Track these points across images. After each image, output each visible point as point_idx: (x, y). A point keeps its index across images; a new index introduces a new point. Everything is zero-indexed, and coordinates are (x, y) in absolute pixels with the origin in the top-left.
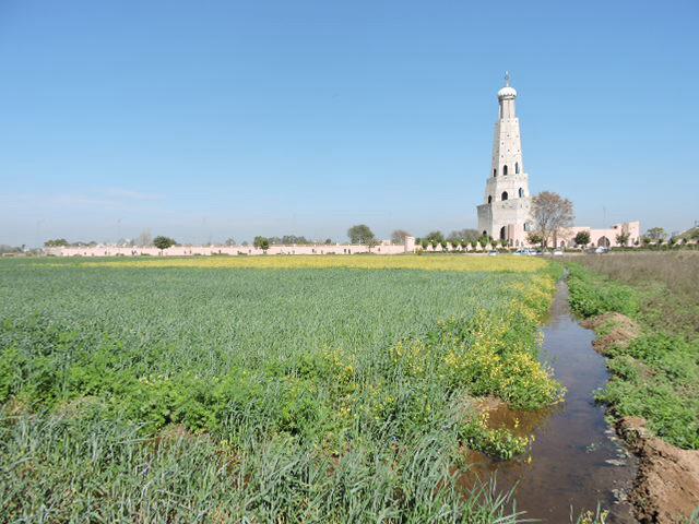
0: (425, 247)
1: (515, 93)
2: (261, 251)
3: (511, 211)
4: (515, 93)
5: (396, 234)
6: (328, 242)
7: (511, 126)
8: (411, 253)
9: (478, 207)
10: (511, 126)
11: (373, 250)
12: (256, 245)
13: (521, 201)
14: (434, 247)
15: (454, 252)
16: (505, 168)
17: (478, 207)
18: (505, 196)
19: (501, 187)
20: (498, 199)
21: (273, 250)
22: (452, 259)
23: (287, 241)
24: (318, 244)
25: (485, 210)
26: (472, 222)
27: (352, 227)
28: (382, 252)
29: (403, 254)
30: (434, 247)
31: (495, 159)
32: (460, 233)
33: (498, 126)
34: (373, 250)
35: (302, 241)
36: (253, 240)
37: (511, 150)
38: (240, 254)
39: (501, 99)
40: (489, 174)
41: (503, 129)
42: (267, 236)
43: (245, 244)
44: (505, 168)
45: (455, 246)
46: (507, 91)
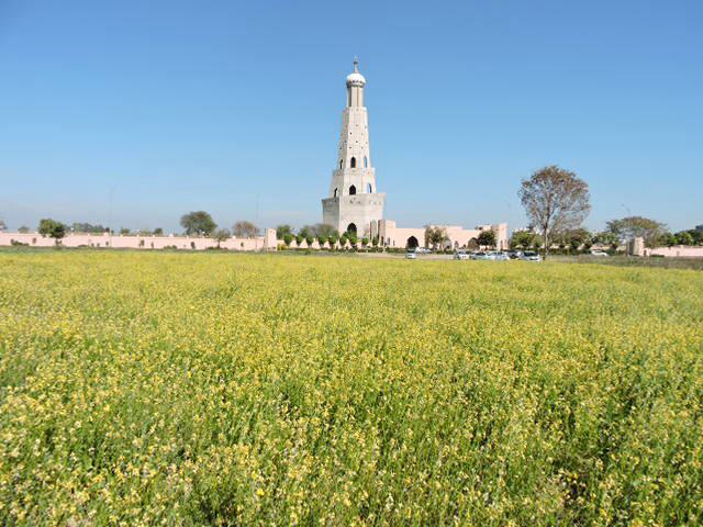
0: (288, 242)
1: (364, 81)
2: (50, 241)
3: (360, 207)
4: (364, 81)
5: (239, 226)
6: (158, 232)
7: (359, 116)
8: (271, 252)
9: (324, 202)
10: (359, 116)
11: (223, 245)
12: (43, 232)
13: (369, 197)
14: (298, 243)
15: (342, 251)
16: (353, 160)
17: (324, 202)
18: (353, 190)
19: (348, 180)
20: (346, 192)
21: (70, 240)
22: (304, 262)
23: (87, 229)
24: (147, 234)
25: (331, 205)
26: (314, 217)
27: (189, 214)
28: (246, 248)
29: (262, 251)
30: (298, 243)
31: (343, 148)
32: (313, 229)
33: (346, 114)
34: (223, 245)
35: (99, 230)
36: (38, 225)
37: (359, 143)
38: (15, 244)
39: (349, 85)
40: (336, 166)
41: (351, 118)
42: (66, 222)
43: (24, 230)
44: (353, 160)
45: (321, 243)
46: (356, 77)
